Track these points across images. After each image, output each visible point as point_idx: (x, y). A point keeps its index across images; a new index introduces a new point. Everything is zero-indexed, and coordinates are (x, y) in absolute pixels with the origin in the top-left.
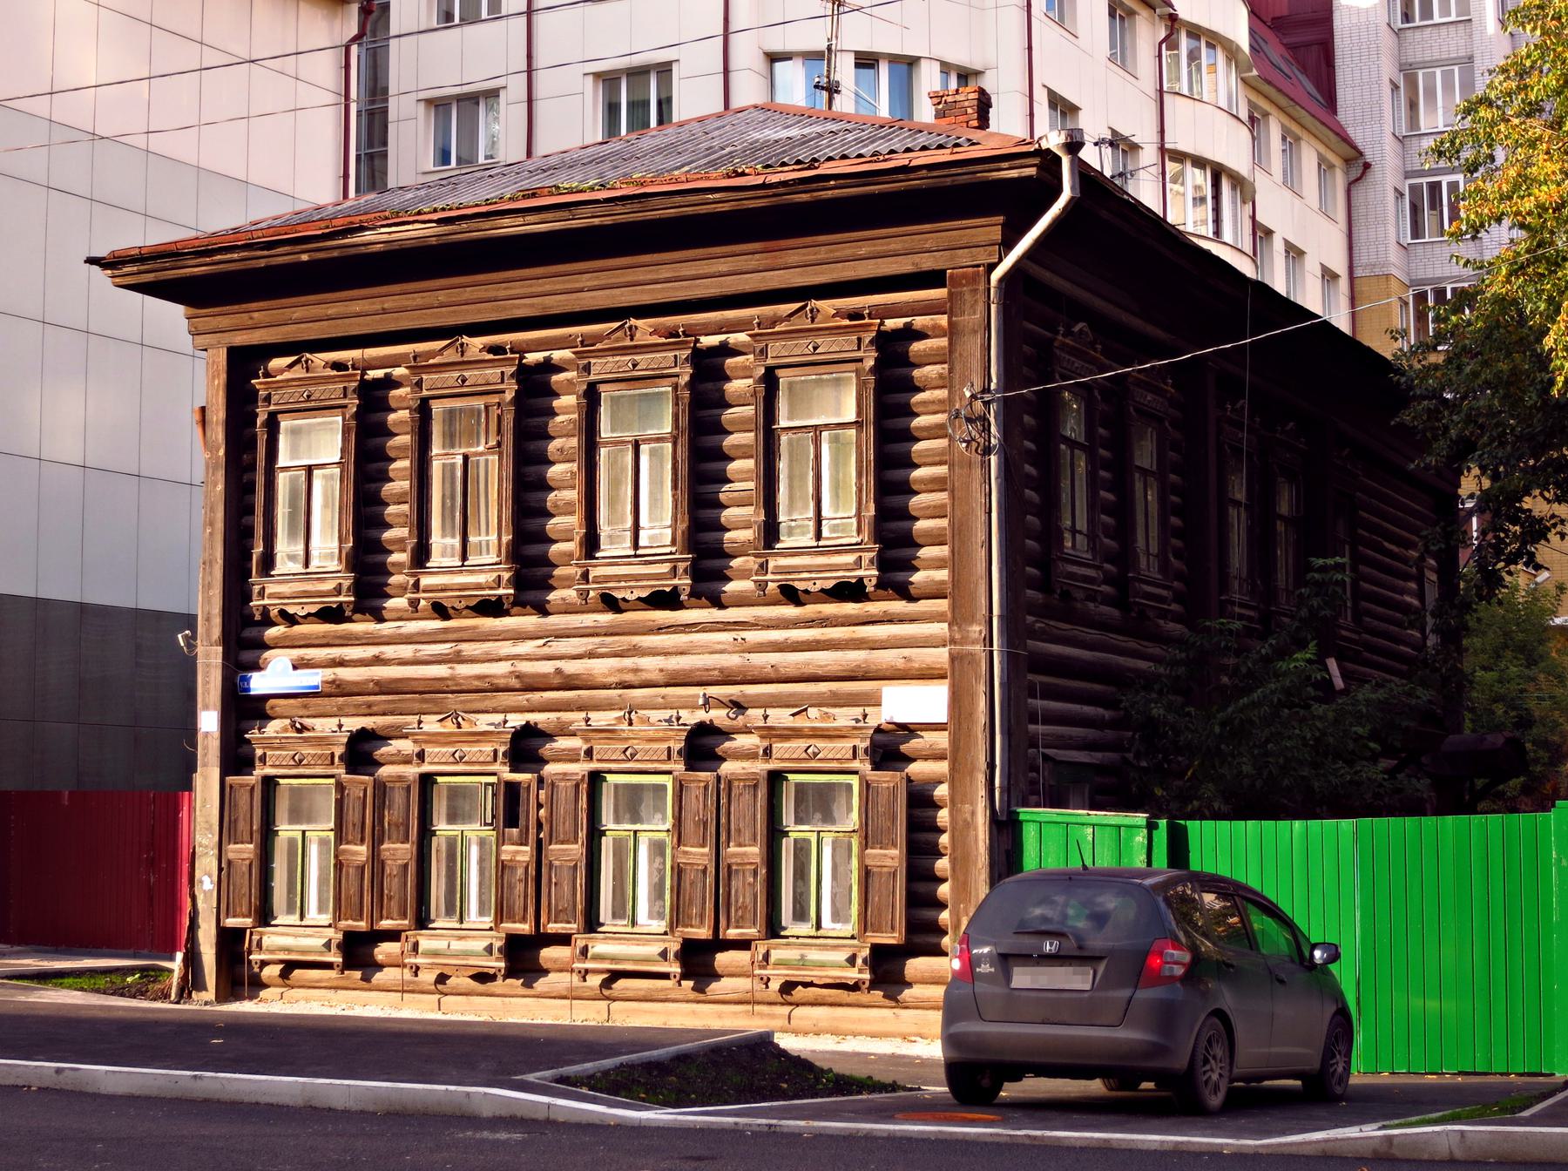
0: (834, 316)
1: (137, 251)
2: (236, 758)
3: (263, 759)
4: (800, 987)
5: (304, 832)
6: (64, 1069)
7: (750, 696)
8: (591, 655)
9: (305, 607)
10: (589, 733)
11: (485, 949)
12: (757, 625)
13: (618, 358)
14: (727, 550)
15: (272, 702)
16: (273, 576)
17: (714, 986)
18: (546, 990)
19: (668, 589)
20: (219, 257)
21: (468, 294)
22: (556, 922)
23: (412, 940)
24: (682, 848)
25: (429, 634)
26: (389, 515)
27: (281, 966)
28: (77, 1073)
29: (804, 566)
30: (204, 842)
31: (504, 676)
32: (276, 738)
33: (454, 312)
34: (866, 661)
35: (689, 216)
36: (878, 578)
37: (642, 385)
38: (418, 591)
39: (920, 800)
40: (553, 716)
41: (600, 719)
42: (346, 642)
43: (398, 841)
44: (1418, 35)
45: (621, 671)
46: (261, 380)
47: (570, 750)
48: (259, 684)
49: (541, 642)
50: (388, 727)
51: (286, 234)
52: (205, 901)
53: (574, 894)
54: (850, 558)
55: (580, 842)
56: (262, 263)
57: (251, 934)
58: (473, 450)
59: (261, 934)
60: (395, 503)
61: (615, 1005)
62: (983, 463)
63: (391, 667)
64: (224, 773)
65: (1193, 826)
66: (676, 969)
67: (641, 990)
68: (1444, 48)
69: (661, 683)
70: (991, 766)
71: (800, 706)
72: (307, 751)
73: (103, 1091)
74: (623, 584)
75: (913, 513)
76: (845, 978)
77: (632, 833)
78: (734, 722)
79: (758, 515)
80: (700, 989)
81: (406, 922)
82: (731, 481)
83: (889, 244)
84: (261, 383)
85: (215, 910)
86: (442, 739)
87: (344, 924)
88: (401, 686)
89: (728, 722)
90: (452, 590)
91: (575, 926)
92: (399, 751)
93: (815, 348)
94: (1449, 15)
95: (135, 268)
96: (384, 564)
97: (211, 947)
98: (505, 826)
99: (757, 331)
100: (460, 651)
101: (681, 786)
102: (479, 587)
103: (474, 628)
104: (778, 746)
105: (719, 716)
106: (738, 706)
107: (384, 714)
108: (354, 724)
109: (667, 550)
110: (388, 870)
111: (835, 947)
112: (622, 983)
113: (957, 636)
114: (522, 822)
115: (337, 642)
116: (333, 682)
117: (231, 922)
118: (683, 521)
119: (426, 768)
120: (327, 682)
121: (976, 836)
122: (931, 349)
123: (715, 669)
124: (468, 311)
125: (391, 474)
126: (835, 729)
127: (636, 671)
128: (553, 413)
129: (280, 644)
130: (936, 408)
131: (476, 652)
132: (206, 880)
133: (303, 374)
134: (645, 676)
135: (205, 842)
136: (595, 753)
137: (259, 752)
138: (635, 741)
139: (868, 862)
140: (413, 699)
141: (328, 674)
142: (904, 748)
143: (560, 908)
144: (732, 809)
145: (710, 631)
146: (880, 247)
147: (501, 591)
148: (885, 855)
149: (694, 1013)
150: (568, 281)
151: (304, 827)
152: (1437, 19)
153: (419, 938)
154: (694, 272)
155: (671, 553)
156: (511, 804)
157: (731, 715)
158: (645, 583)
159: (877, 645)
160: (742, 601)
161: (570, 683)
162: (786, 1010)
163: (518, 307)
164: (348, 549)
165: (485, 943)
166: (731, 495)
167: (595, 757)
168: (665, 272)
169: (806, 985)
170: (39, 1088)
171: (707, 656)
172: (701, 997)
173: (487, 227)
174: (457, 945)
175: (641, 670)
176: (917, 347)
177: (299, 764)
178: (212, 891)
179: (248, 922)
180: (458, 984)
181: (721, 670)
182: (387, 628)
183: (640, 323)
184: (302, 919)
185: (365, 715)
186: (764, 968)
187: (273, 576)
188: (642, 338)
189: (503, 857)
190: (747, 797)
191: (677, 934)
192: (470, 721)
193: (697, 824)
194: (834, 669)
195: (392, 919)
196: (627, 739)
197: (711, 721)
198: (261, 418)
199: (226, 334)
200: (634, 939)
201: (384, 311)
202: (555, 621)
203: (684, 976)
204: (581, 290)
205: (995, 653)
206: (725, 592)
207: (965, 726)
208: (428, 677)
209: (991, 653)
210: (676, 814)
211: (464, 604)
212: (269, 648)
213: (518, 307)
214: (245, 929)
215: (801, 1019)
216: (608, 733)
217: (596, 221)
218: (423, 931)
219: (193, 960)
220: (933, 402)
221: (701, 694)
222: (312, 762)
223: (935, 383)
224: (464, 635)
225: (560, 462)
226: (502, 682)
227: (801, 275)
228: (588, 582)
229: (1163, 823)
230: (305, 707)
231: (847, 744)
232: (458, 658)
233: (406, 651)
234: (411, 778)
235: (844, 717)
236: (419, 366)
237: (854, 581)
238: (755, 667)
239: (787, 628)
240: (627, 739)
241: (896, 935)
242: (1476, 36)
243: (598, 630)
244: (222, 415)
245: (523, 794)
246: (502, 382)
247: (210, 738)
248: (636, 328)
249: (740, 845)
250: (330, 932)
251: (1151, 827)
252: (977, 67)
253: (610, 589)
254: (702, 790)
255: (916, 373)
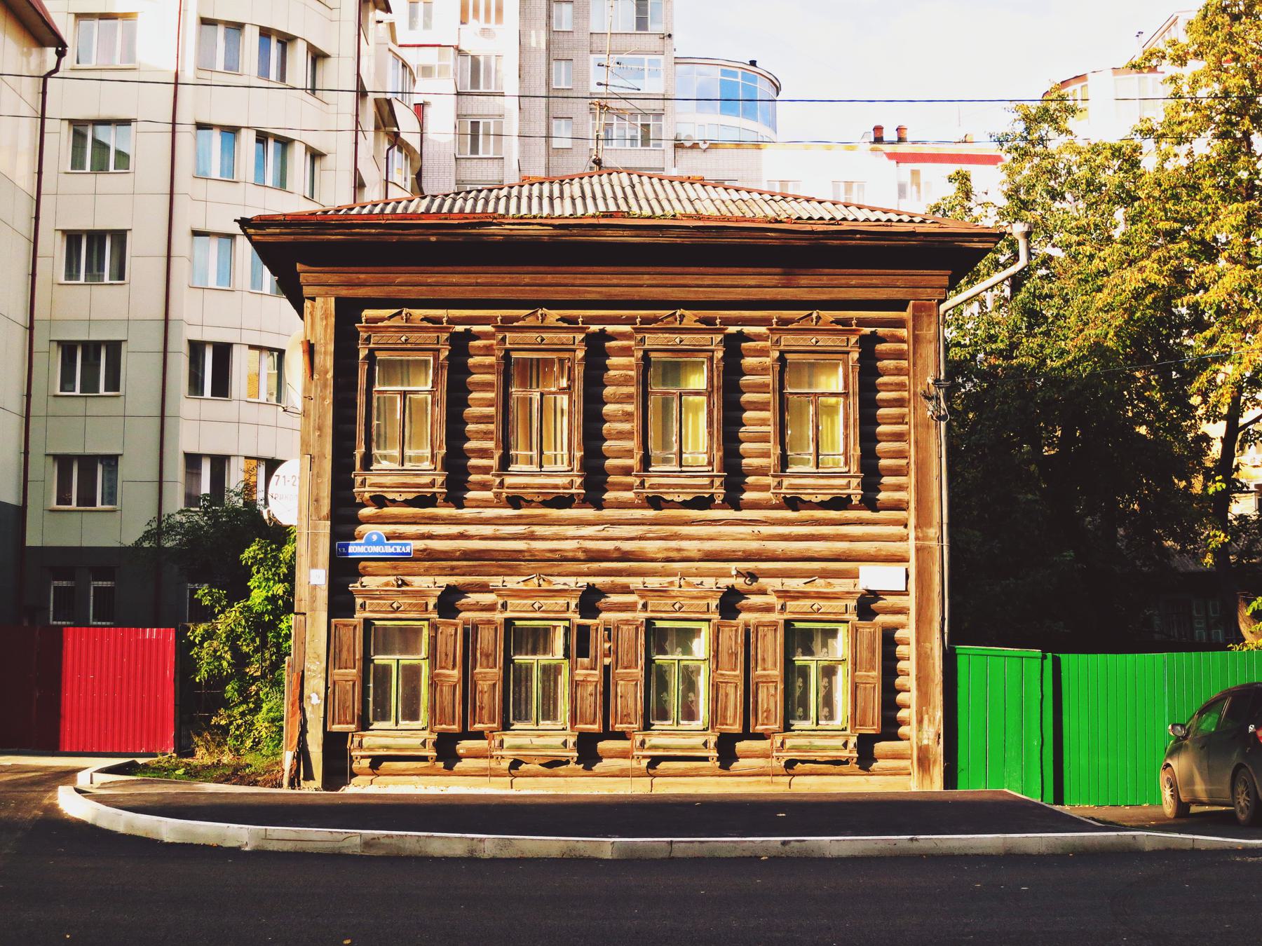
0: (832, 322)
1: (282, 218)
2: (340, 603)
3: (363, 606)
4: (799, 764)
5: (398, 660)
6: (789, 841)
7: (762, 569)
8: (641, 538)
9: (681, 496)
10: (645, 592)
11: (563, 744)
12: (766, 522)
13: (667, 335)
14: (744, 472)
15: (362, 564)
16: (372, 470)
17: (458, 765)
18: (602, 771)
19: (707, 496)
20: (357, 230)
21: (549, 279)
22: (621, 723)
23: (500, 738)
24: (719, 672)
25: (506, 518)
26: (469, 431)
27: (370, 760)
28: (803, 844)
29: (809, 485)
30: (312, 668)
31: (573, 551)
32: (377, 590)
33: (537, 291)
34: (849, 549)
35: (750, 245)
36: (725, 494)
37: (685, 355)
38: (503, 488)
39: (889, 640)
40: (608, 580)
41: (654, 582)
42: (431, 522)
43: (488, 667)
44: (468, 163)
45: (667, 550)
46: (363, 324)
47: (621, 604)
48: (355, 549)
49: (601, 527)
50: (469, 584)
51: (411, 219)
52: (313, 712)
53: (636, 705)
54: (843, 482)
55: (639, 668)
56: (395, 239)
57: (353, 736)
58: (546, 389)
59: (362, 736)
60: (473, 423)
61: (656, 780)
62: (936, 426)
63: (474, 541)
64: (330, 617)
65: (1064, 658)
66: (432, 753)
67: (679, 769)
68: (485, 174)
69: (697, 558)
70: (943, 619)
71: (810, 575)
72: (404, 601)
73: (828, 855)
74: (671, 490)
75: (878, 455)
76: (840, 757)
77: (676, 662)
78: (750, 587)
79: (773, 448)
80: (449, 767)
81: (495, 725)
82: (745, 425)
83: (872, 279)
84: (360, 327)
85: (322, 719)
86: (524, 594)
87: (438, 727)
88: (496, 555)
89: (746, 587)
90: (532, 488)
91: (636, 726)
92: (478, 602)
93: (817, 342)
94: (489, 153)
95: (278, 231)
96: (465, 467)
97: (318, 745)
98: (577, 657)
99: (774, 326)
100: (533, 532)
101: (718, 629)
102: (556, 487)
103: (544, 515)
104: (792, 605)
105: (739, 583)
106: (753, 576)
107: (463, 575)
108: (444, 581)
109: (706, 469)
110: (479, 688)
111: (833, 737)
112: (663, 765)
113: (920, 535)
114: (592, 652)
115: (423, 521)
116: (424, 550)
117: (336, 728)
118: (718, 450)
119: (508, 614)
120: (418, 550)
121: (934, 663)
122: (890, 350)
123: (740, 551)
124: (547, 291)
125: (470, 402)
126: (835, 593)
127: (679, 550)
128: (606, 369)
129: (370, 520)
130: (893, 388)
131: (547, 533)
132: (314, 697)
133: (403, 323)
134: (685, 554)
135: (312, 667)
136: (367, 606)
137: (359, 601)
138: (681, 598)
139: (857, 680)
140: (492, 565)
141: (420, 544)
142: (873, 606)
143: (625, 713)
144: (759, 645)
145: (730, 525)
146: (866, 281)
147: (573, 491)
148: (868, 676)
149: (718, 783)
150: (632, 279)
151: (398, 657)
152: (481, 155)
153: (504, 737)
154: (730, 283)
155: (708, 471)
156: (581, 643)
157: (747, 581)
158: (688, 490)
159: (855, 539)
160: (755, 505)
161: (625, 556)
162: (787, 779)
163: (589, 292)
164: (443, 455)
165: (562, 739)
166: (747, 435)
167: (367, 609)
168: (708, 280)
169: (803, 762)
170: (770, 857)
171: (731, 541)
172: (726, 772)
173: (593, 234)
174: (538, 742)
175: (683, 550)
176: (881, 347)
177: (397, 610)
178: (319, 705)
179: (352, 727)
180: (529, 770)
181: (744, 552)
182: (467, 513)
183: (687, 313)
184: (397, 725)
185: (446, 575)
186: (780, 751)
187: (372, 470)
188: (687, 324)
189: (577, 678)
190: (770, 636)
191: (716, 730)
192: (550, 582)
193: (730, 655)
194: (826, 554)
195: (483, 723)
196: (674, 597)
197: (733, 586)
198: (363, 353)
199: (333, 288)
200: (682, 734)
201: (477, 284)
202: (607, 513)
203: (438, 759)
204: (641, 286)
205: (945, 548)
206: (742, 499)
207: (925, 593)
208: (508, 549)
209: (942, 546)
210: (715, 648)
211: (541, 498)
212: (362, 523)
213: (589, 292)
214: (347, 733)
215: (798, 785)
216: (662, 592)
217: (679, 240)
218: (508, 732)
219: (302, 754)
220: (891, 384)
221: (734, 568)
222: (409, 609)
223: (892, 372)
224: (535, 520)
225: (611, 403)
226: (570, 554)
227: (807, 292)
228: (644, 488)
229: (1049, 655)
230: (395, 568)
231: (841, 603)
232: (532, 537)
233: (488, 530)
234: (499, 622)
235: (840, 585)
236: (506, 325)
237: (845, 496)
238: (769, 550)
239: (820, 525)
240: (674, 597)
241: (876, 727)
242: (506, 169)
243: (645, 521)
244: (331, 348)
245: (592, 634)
246: (438, 343)
247: (318, 590)
248: (684, 316)
249: (764, 669)
250: (426, 734)
251: (1044, 658)
252: (324, 151)
253: (661, 493)
254: (734, 632)
255: (879, 364)
